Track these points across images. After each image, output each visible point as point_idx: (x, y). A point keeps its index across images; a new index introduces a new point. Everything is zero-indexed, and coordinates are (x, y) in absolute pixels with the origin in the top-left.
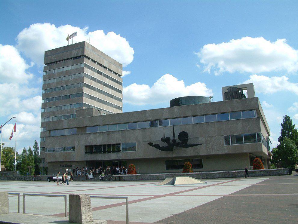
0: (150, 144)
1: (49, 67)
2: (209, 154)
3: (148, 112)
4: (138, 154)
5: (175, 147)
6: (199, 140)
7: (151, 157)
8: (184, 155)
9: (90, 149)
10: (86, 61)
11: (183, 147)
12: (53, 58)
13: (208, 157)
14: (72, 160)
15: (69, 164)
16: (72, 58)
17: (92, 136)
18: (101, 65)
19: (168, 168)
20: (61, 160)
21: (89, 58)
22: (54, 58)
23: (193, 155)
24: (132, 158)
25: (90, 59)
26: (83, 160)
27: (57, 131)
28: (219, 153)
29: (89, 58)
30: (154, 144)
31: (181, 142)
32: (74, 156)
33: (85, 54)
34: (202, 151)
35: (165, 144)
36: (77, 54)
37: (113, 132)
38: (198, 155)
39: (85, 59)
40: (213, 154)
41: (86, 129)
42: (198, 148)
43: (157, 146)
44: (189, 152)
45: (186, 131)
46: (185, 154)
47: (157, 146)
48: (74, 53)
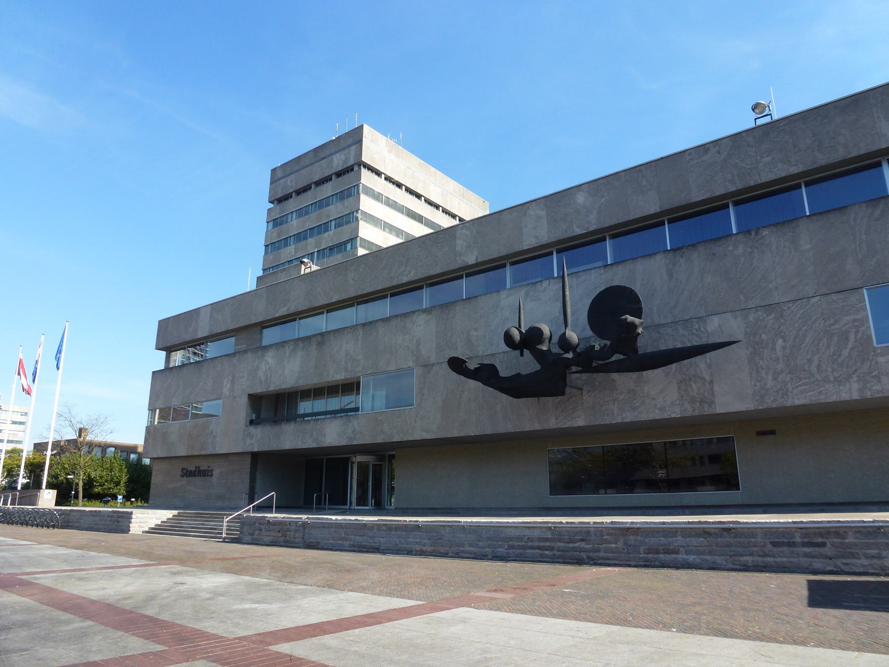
0: (457, 365)
1: (278, 207)
2: (771, 402)
3: (464, 231)
4: (422, 423)
5: (576, 377)
6: (709, 329)
7: (472, 431)
8: (629, 417)
9: (272, 406)
10: (365, 174)
11: (621, 368)
12: (289, 183)
13: (768, 426)
14: (210, 451)
15: (204, 466)
16: (334, 177)
17: (270, 358)
18: (419, 196)
19: (556, 488)
20: (182, 452)
21: (378, 173)
22: (291, 181)
23: (676, 413)
24: (396, 439)
25: (383, 176)
26: (239, 450)
27: (740, 502)
28: (845, 396)
29: (378, 173)
30: (472, 365)
31: (608, 343)
32: (214, 437)
33: (365, 158)
34: (731, 389)
35: (527, 364)
36: (346, 161)
37: (335, 331)
38: (707, 410)
39: (364, 172)
40: (798, 402)
41: (261, 333)
42: (708, 378)
43: (486, 374)
44: (655, 399)
45: (638, 289)
46: (634, 409)
47: (486, 374)
48: (338, 162)
